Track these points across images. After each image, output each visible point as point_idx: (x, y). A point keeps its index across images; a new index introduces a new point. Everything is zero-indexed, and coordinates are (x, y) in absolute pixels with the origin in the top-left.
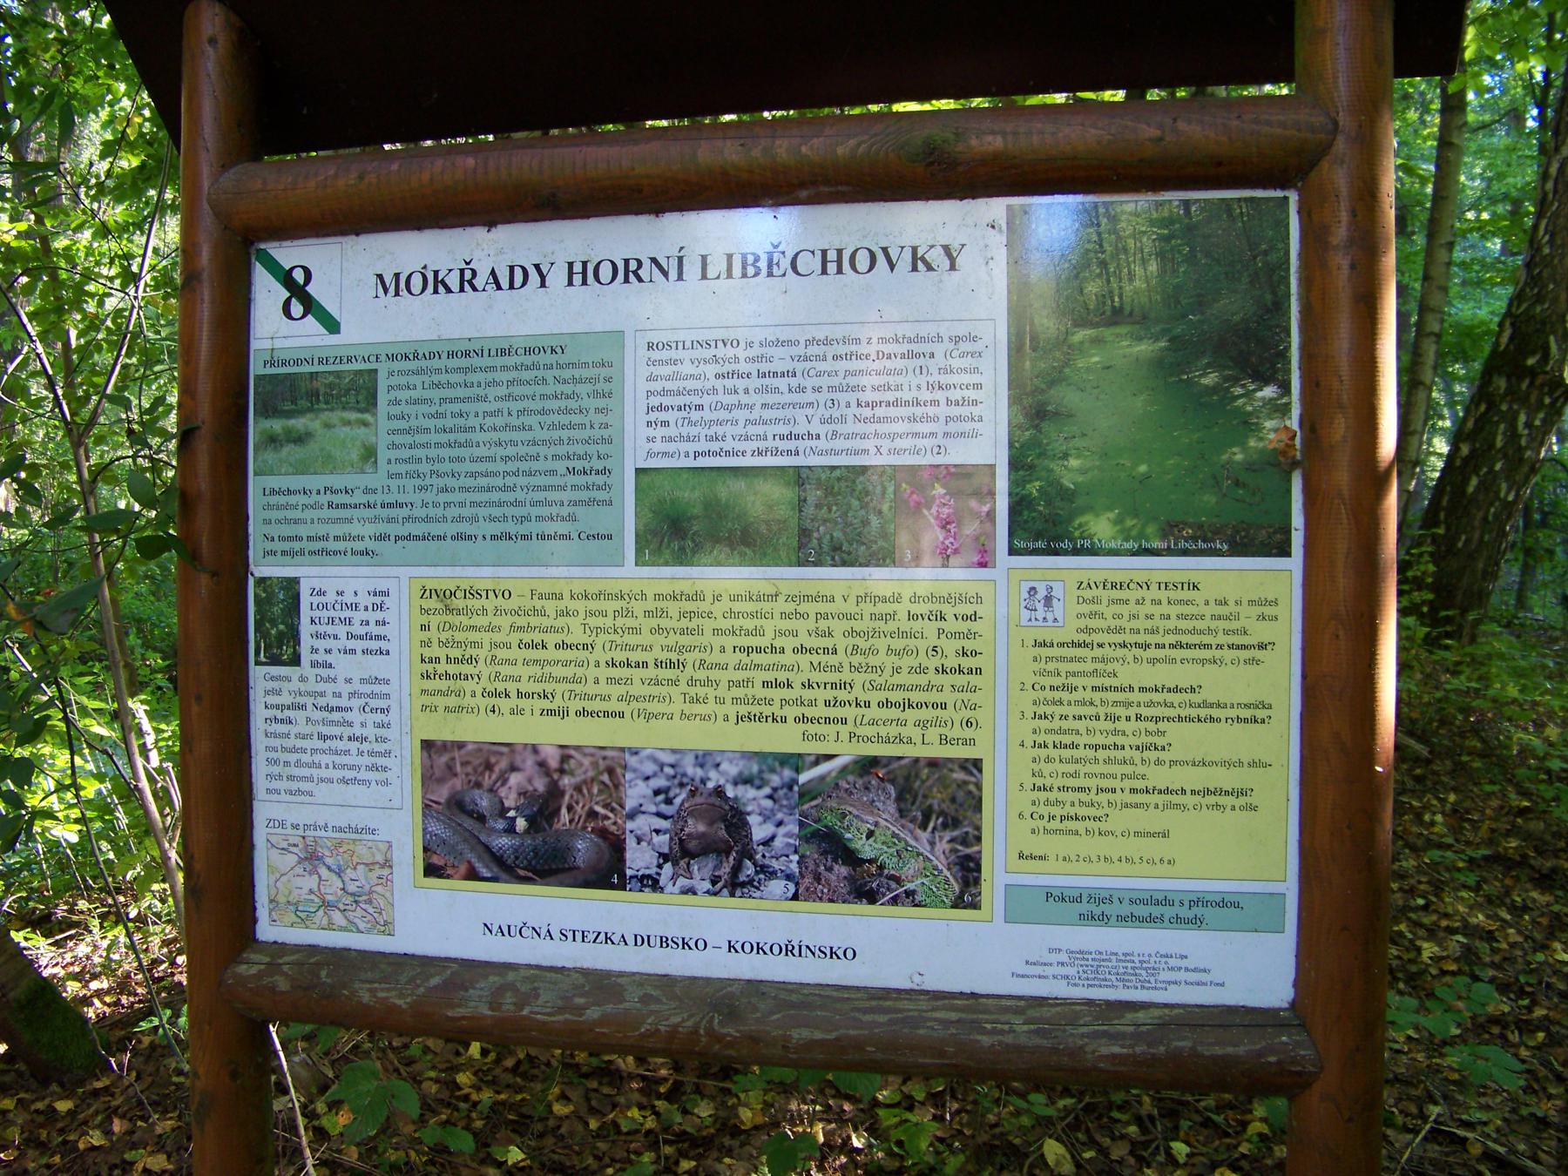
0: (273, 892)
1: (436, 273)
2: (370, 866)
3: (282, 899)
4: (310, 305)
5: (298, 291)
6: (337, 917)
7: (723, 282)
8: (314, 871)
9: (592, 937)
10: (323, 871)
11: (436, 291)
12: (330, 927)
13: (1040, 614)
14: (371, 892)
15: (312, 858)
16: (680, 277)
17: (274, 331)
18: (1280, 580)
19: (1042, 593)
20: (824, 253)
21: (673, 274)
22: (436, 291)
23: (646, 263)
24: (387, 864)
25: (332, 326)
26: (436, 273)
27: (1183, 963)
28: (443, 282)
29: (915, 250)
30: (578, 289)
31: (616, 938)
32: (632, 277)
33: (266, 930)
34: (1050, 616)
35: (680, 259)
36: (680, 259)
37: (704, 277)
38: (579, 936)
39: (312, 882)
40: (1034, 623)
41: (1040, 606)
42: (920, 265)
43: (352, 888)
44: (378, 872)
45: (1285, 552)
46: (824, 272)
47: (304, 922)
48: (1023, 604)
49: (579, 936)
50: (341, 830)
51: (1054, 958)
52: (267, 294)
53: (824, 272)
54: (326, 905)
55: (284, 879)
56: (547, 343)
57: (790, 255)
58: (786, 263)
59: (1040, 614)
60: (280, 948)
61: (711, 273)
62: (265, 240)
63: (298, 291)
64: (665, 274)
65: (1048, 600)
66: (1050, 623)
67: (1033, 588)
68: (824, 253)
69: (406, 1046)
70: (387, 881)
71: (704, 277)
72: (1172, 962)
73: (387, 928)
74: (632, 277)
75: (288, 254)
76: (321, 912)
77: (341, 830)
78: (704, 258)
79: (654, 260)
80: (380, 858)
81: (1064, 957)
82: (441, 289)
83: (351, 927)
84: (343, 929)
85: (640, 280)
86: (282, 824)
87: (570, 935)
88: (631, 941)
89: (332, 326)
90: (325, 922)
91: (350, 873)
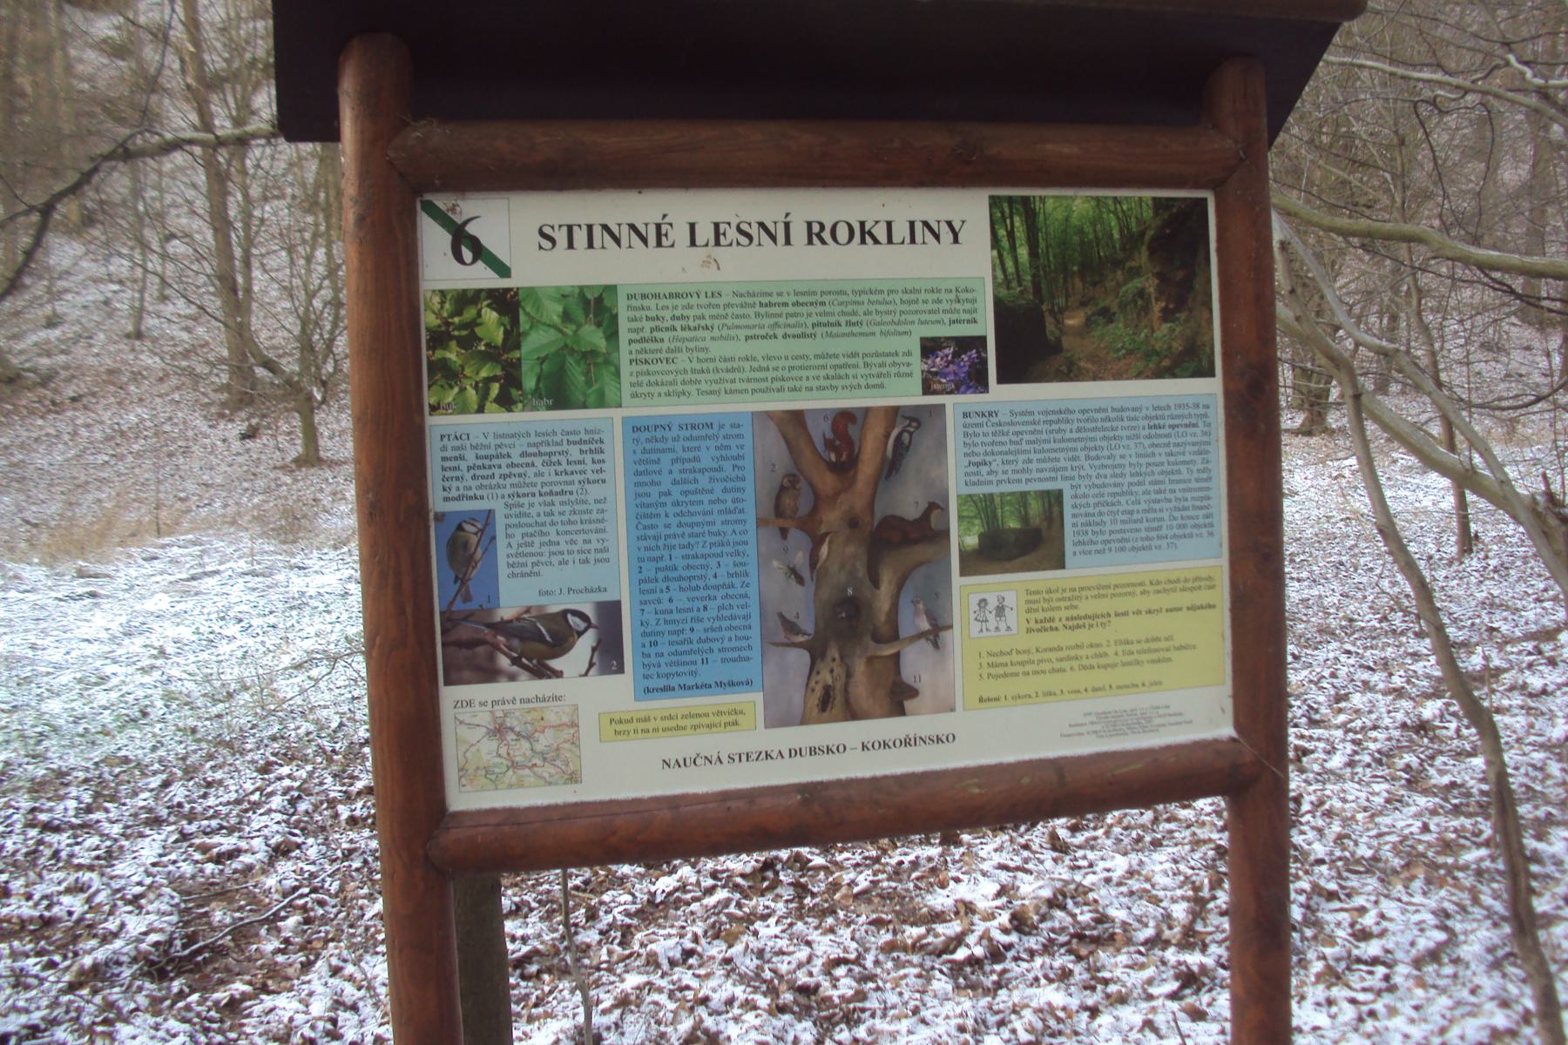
0: (462, 762)
1: (862, 224)
4: (479, 251)
5: (464, 242)
9: (754, 756)
11: (863, 241)
13: (992, 623)
14: (558, 749)
16: (788, 242)
17: (441, 270)
18: (1209, 390)
19: (993, 604)
22: (863, 241)
24: (574, 725)
25: (503, 270)
26: (862, 224)
28: (870, 233)
31: (774, 755)
32: (815, 239)
34: (1002, 626)
35: (787, 225)
36: (787, 225)
37: (693, 243)
38: (744, 758)
40: (985, 633)
41: (991, 617)
42: (868, 239)
45: (1212, 375)
47: (496, 785)
48: (973, 616)
49: (744, 758)
50: (529, 701)
51: (1088, 719)
52: (433, 240)
54: (514, 765)
55: (473, 749)
56: (692, 289)
59: (992, 623)
61: (699, 241)
62: (428, 191)
63: (464, 242)
64: (773, 238)
65: (1000, 611)
66: (1003, 631)
67: (984, 600)
70: (575, 742)
71: (693, 243)
72: (1161, 711)
74: (815, 239)
76: (510, 772)
77: (529, 701)
78: (692, 226)
79: (926, 224)
80: (565, 719)
81: (1094, 719)
82: (868, 239)
87: (561, 236)
88: (786, 754)
90: (514, 780)
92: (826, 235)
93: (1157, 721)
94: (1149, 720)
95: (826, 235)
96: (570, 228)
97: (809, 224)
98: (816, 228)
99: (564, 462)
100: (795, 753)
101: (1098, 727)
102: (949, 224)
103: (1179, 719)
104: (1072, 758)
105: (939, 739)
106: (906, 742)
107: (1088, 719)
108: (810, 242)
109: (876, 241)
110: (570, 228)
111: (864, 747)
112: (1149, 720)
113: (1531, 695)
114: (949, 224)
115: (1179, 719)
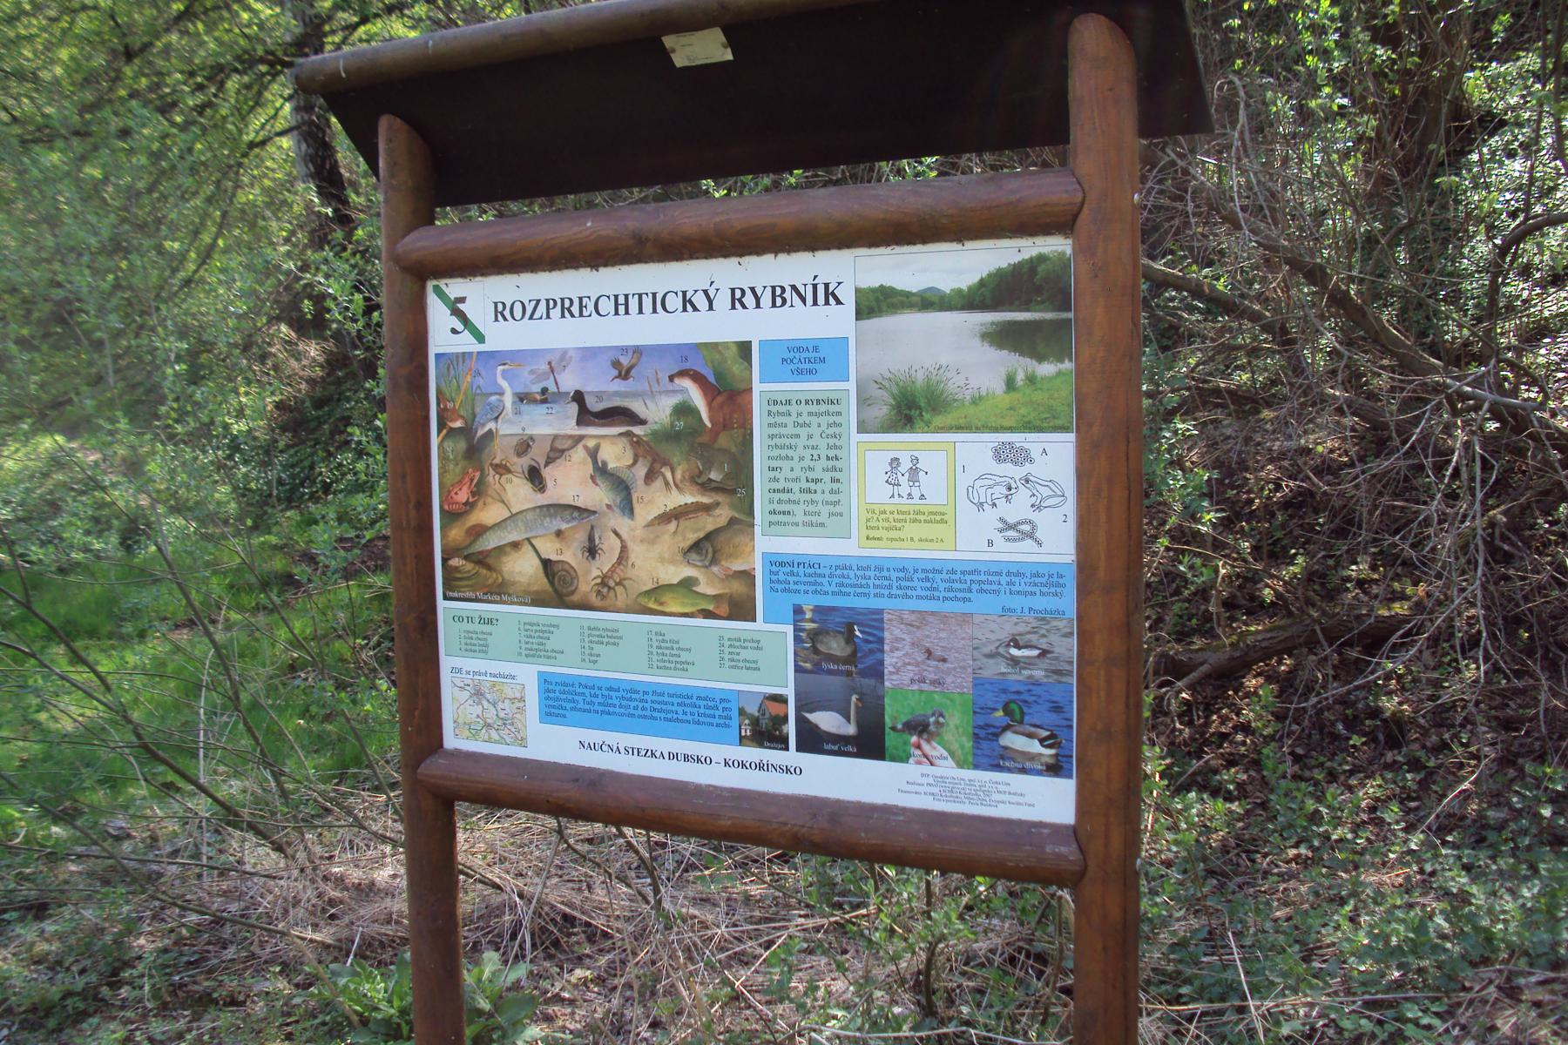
1: (827, 286)
2: (512, 700)
3: (461, 721)
6: (494, 734)
7: (544, 321)
8: (480, 703)
10: (485, 704)
11: (827, 303)
12: (489, 741)
13: (905, 489)
15: (478, 694)
19: (906, 465)
20: (616, 297)
21: (809, 300)
22: (827, 303)
23: (788, 289)
24: (522, 700)
25: (480, 338)
26: (827, 286)
27: (1007, 789)
29: (684, 293)
30: (622, 317)
32: (737, 304)
33: (451, 741)
34: (916, 493)
39: (478, 710)
40: (897, 500)
41: (904, 480)
42: (831, 300)
43: (502, 715)
44: (517, 704)
46: (617, 313)
47: (475, 735)
51: (925, 780)
52: (439, 318)
53: (617, 313)
54: (489, 726)
57: (593, 300)
58: (591, 307)
60: (457, 754)
64: (804, 300)
65: (914, 472)
68: (616, 297)
69: (1401, 704)
70: (521, 710)
73: (522, 742)
74: (737, 304)
75: (455, 287)
79: (794, 288)
80: (518, 695)
81: (931, 780)
82: (831, 300)
83: (502, 741)
84: (496, 742)
85: (744, 307)
86: (460, 671)
89: (480, 338)
91: (500, 706)
92: (507, 313)
93: (996, 797)
94: (987, 793)
95: (507, 313)
96: (640, 296)
97: (733, 290)
98: (778, 291)
99: (796, 490)
100: (673, 756)
101: (936, 790)
102: (753, 290)
103: (1020, 799)
104: (787, 798)
105: (788, 770)
106: (687, 758)
107: (925, 780)
108: (733, 307)
109: (695, 309)
110: (640, 296)
111: (726, 763)
112: (987, 793)
113: (1356, 853)
114: (753, 290)
115: (1020, 799)
